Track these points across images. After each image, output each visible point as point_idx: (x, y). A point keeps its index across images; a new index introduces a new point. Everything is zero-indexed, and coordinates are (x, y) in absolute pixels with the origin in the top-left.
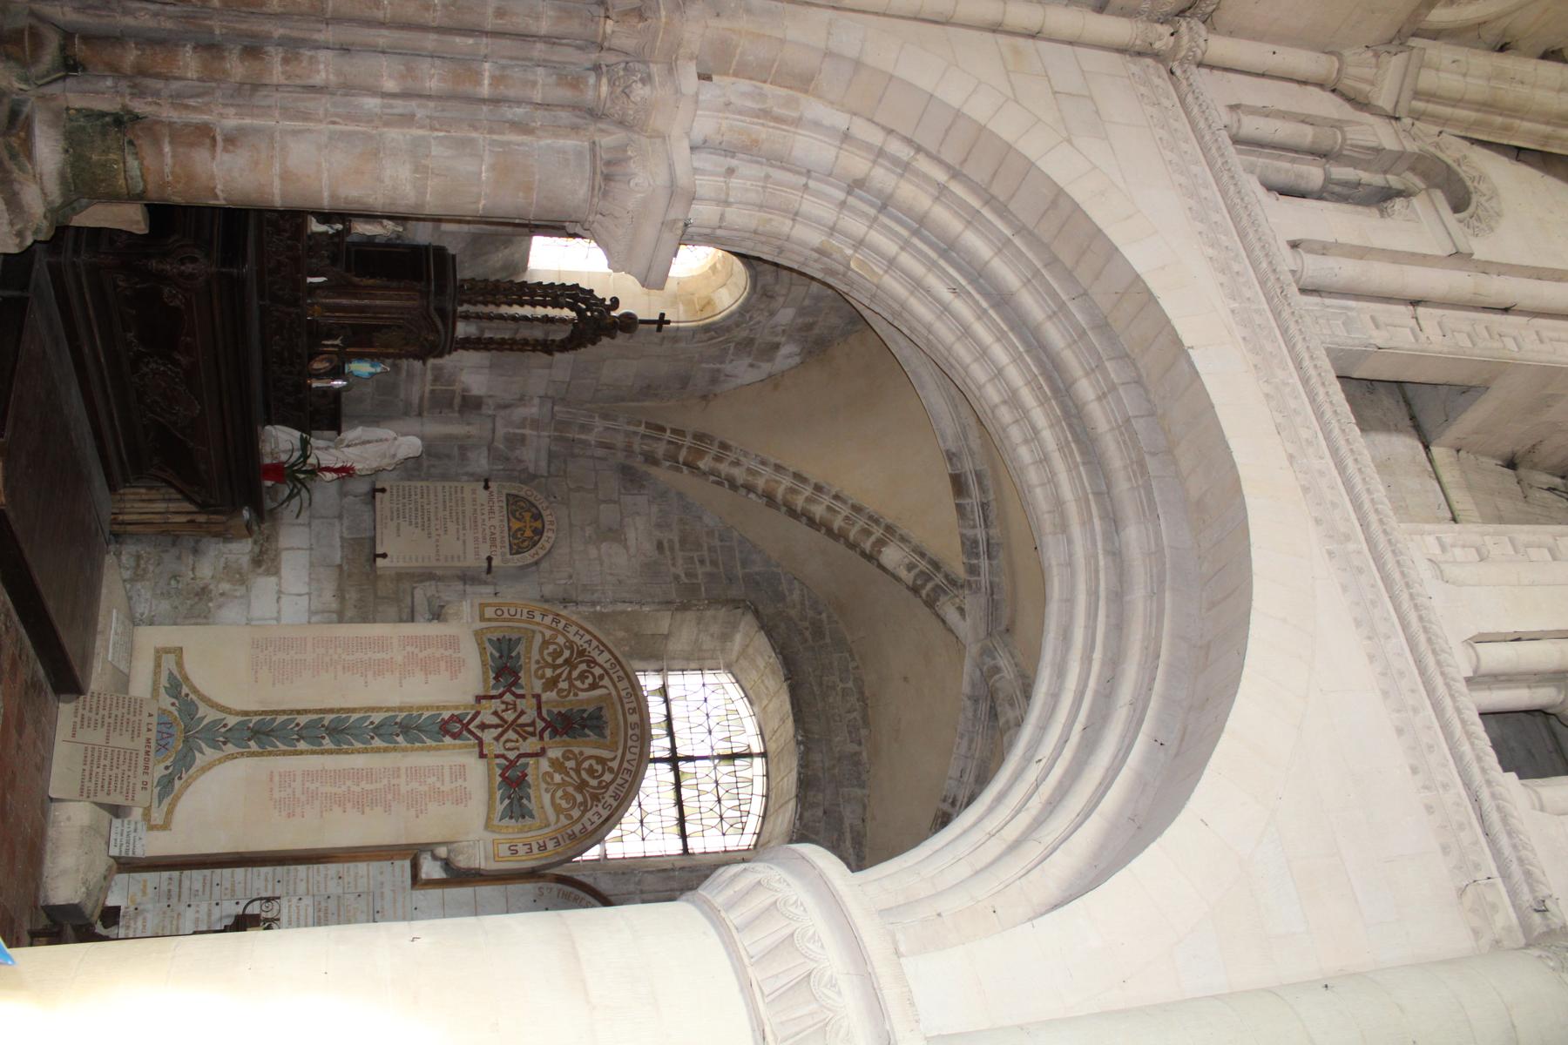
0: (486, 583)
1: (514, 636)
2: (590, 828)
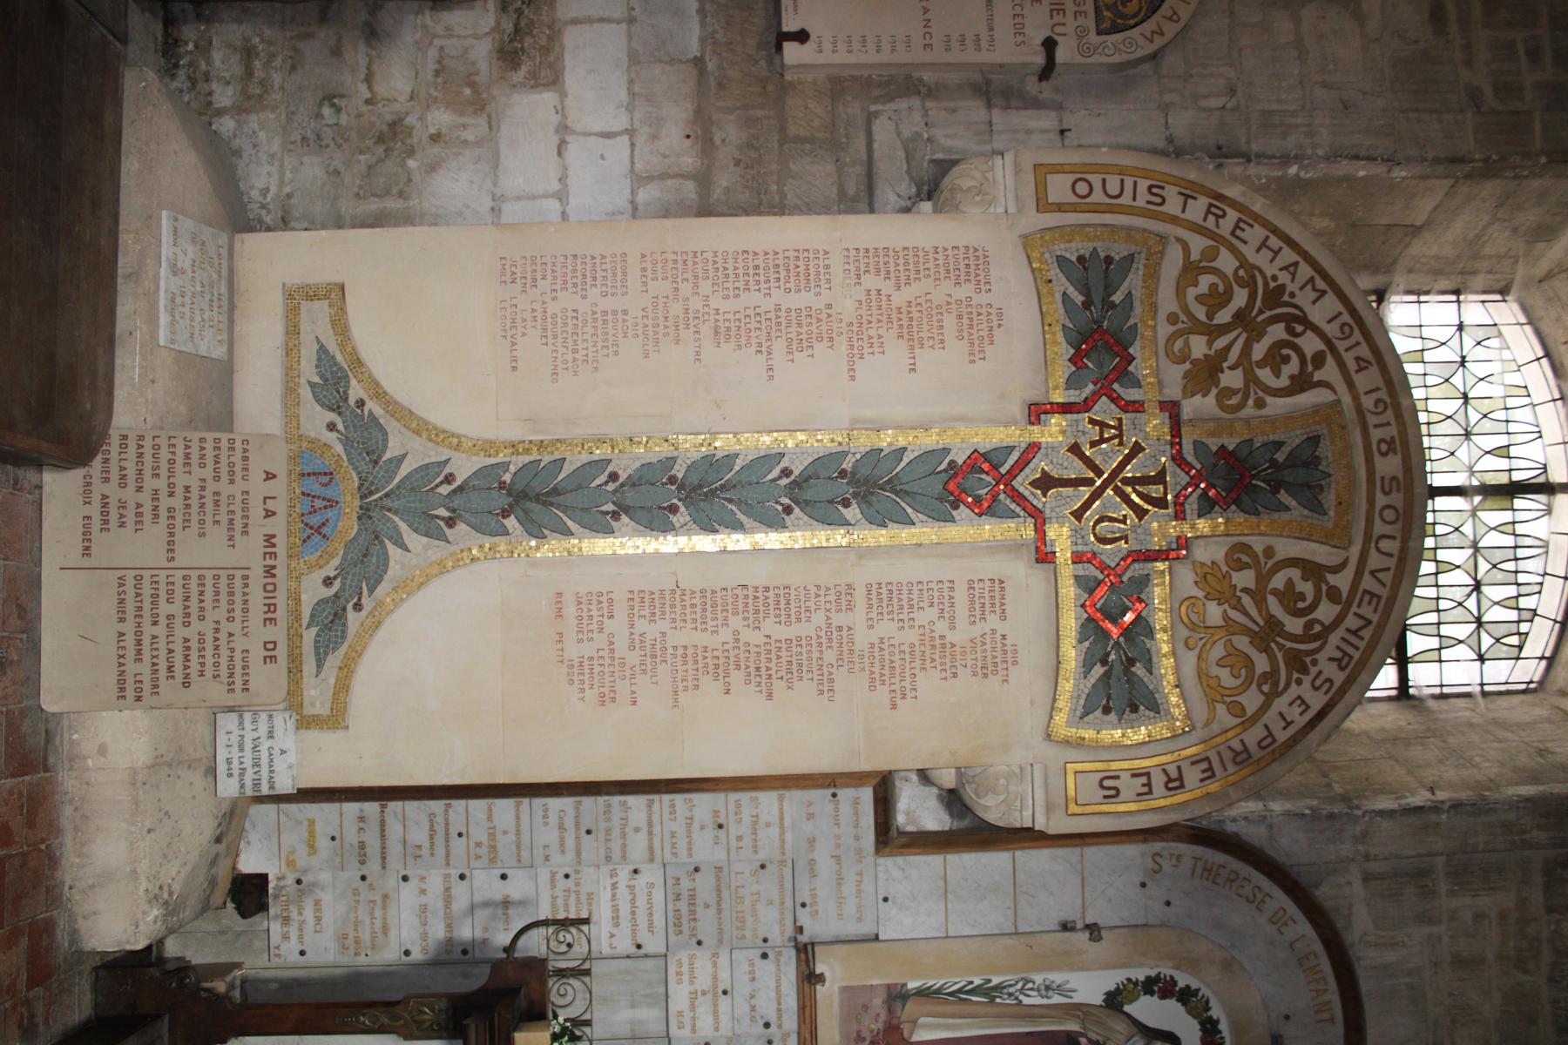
0: (1036, 104)
1: (1119, 251)
2: (1282, 736)
